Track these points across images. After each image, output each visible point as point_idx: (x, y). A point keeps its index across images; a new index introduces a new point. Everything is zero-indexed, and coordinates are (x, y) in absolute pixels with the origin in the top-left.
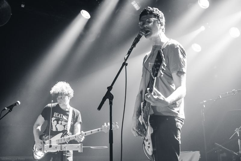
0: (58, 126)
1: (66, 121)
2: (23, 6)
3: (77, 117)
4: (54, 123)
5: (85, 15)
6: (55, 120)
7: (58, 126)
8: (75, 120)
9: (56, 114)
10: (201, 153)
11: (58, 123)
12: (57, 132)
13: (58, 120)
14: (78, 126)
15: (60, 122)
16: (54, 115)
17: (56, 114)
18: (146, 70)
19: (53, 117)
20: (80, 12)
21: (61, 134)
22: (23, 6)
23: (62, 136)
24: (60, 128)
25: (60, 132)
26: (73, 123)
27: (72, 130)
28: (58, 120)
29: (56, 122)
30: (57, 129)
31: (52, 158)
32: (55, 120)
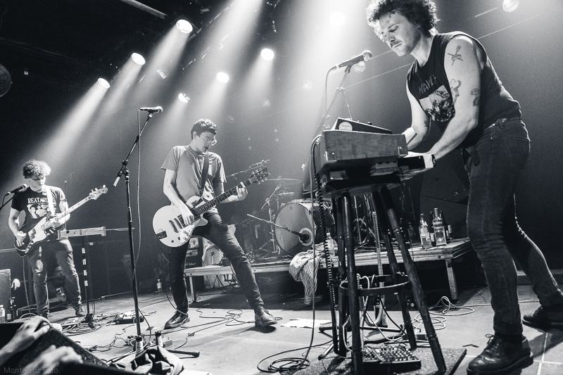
0: (38, 212)
1: (46, 204)
2: (26, 73)
3: (59, 196)
4: (32, 211)
5: (137, 59)
6: (32, 206)
7: (38, 212)
8: (58, 200)
9: (30, 200)
10: (236, 226)
11: (37, 209)
12: (40, 219)
13: (35, 206)
14: (64, 205)
15: (39, 207)
16: (29, 202)
17: (30, 200)
18: (312, 349)
19: (28, 204)
20: (130, 56)
21: (45, 218)
22: (26, 73)
23: (48, 220)
24: (40, 212)
25: (42, 217)
26: (55, 203)
27: (58, 211)
28: (35, 206)
29: (33, 208)
30: (38, 216)
31: (358, 274)
32: (32, 206)
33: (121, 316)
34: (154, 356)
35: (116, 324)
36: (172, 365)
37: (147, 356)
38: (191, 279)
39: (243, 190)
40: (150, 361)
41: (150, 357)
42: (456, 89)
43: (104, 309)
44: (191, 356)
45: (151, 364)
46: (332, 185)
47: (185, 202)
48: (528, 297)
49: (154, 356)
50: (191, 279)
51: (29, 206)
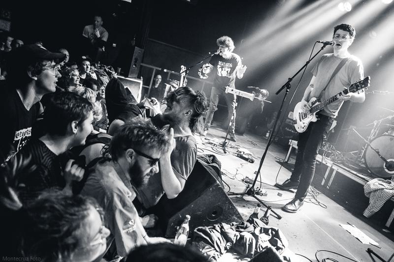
11: (222, 70)
15: (224, 69)
16: (219, 64)
28: (222, 67)
33: (242, 153)
34: (274, 233)
35: (238, 156)
36: (283, 246)
37: (270, 231)
38: (291, 147)
39: (312, 89)
40: (271, 235)
41: (272, 233)
42: (272, 128)
43: (247, 146)
44: (276, 216)
45: (271, 237)
46: (59, 178)
47: (334, 34)
48: (378, 240)
49: (274, 233)
50: (291, 147)
51: (219, 66)
